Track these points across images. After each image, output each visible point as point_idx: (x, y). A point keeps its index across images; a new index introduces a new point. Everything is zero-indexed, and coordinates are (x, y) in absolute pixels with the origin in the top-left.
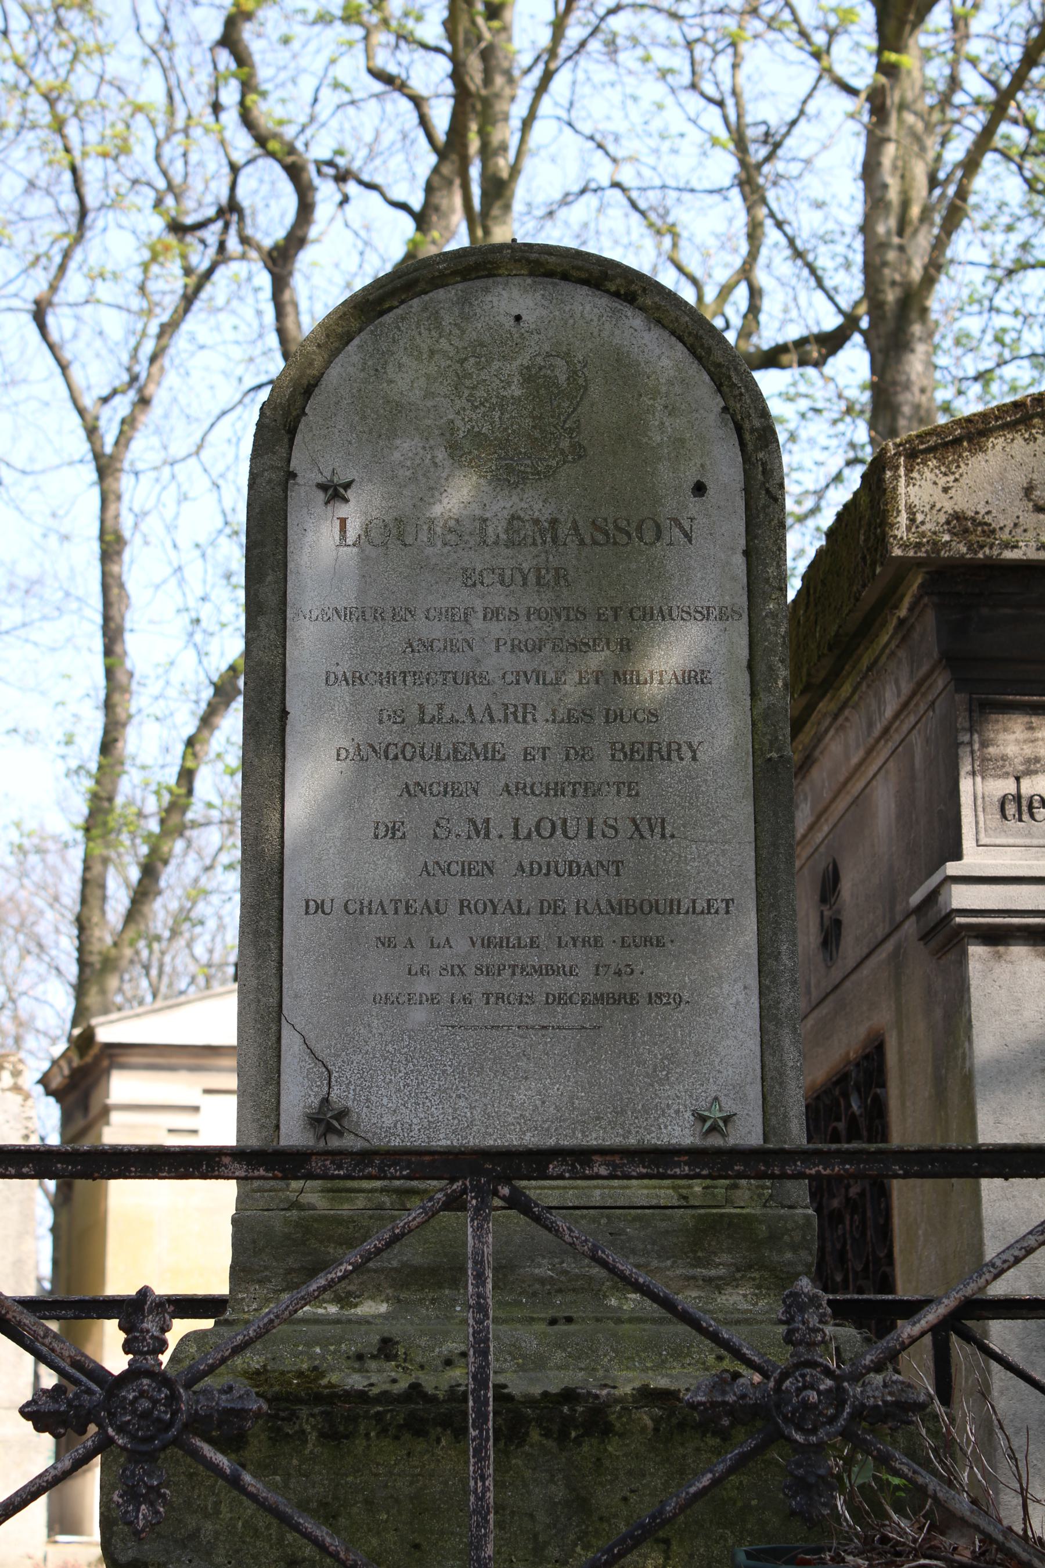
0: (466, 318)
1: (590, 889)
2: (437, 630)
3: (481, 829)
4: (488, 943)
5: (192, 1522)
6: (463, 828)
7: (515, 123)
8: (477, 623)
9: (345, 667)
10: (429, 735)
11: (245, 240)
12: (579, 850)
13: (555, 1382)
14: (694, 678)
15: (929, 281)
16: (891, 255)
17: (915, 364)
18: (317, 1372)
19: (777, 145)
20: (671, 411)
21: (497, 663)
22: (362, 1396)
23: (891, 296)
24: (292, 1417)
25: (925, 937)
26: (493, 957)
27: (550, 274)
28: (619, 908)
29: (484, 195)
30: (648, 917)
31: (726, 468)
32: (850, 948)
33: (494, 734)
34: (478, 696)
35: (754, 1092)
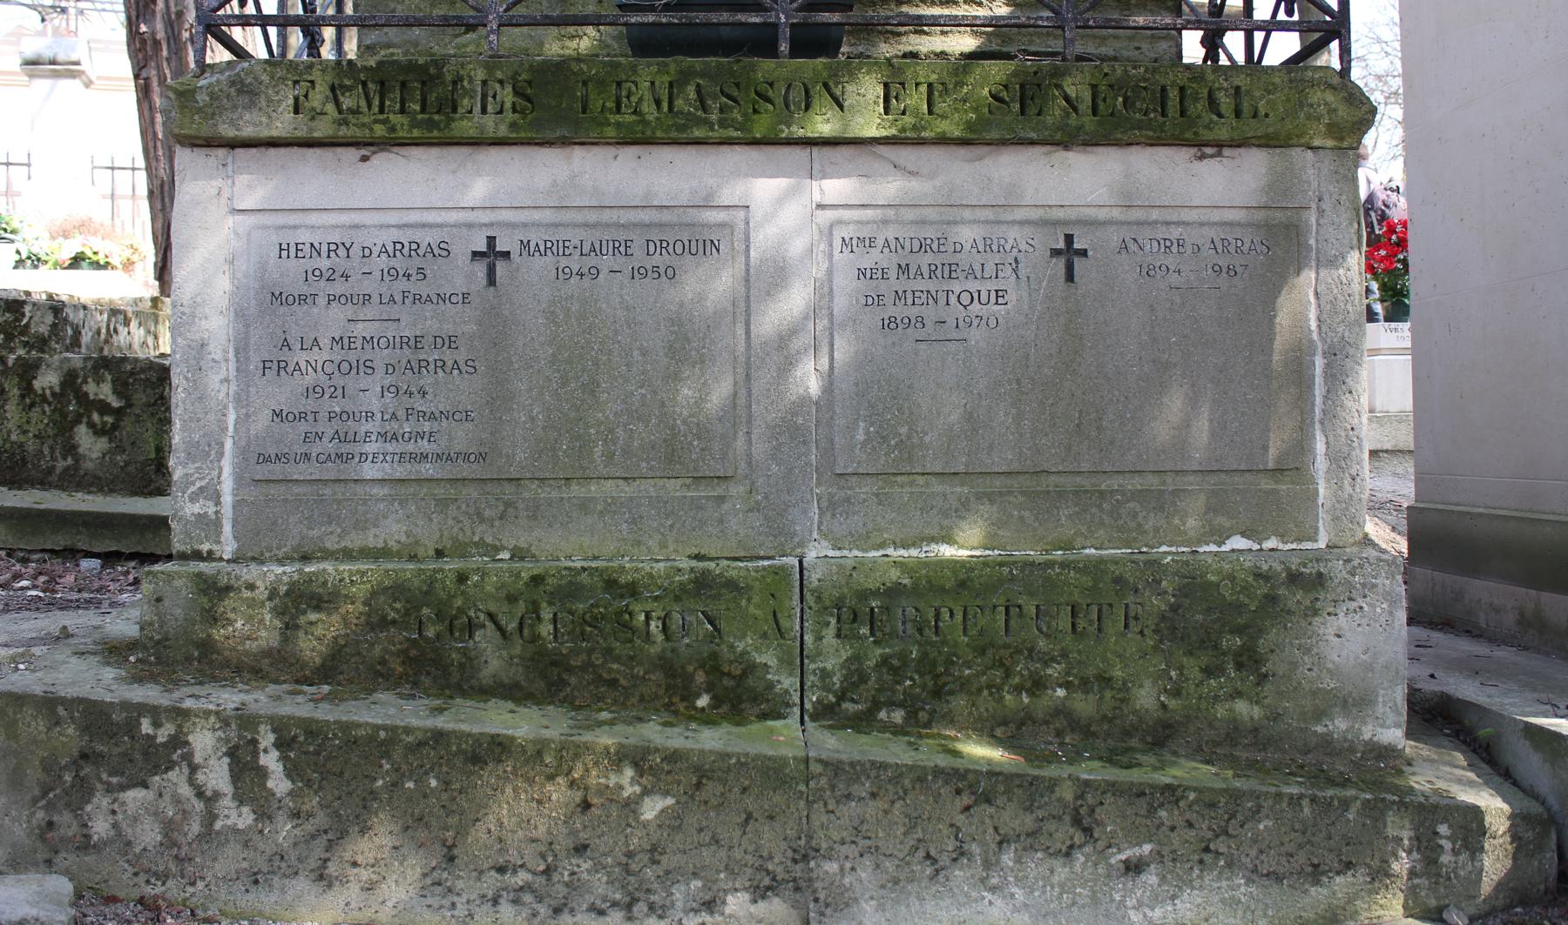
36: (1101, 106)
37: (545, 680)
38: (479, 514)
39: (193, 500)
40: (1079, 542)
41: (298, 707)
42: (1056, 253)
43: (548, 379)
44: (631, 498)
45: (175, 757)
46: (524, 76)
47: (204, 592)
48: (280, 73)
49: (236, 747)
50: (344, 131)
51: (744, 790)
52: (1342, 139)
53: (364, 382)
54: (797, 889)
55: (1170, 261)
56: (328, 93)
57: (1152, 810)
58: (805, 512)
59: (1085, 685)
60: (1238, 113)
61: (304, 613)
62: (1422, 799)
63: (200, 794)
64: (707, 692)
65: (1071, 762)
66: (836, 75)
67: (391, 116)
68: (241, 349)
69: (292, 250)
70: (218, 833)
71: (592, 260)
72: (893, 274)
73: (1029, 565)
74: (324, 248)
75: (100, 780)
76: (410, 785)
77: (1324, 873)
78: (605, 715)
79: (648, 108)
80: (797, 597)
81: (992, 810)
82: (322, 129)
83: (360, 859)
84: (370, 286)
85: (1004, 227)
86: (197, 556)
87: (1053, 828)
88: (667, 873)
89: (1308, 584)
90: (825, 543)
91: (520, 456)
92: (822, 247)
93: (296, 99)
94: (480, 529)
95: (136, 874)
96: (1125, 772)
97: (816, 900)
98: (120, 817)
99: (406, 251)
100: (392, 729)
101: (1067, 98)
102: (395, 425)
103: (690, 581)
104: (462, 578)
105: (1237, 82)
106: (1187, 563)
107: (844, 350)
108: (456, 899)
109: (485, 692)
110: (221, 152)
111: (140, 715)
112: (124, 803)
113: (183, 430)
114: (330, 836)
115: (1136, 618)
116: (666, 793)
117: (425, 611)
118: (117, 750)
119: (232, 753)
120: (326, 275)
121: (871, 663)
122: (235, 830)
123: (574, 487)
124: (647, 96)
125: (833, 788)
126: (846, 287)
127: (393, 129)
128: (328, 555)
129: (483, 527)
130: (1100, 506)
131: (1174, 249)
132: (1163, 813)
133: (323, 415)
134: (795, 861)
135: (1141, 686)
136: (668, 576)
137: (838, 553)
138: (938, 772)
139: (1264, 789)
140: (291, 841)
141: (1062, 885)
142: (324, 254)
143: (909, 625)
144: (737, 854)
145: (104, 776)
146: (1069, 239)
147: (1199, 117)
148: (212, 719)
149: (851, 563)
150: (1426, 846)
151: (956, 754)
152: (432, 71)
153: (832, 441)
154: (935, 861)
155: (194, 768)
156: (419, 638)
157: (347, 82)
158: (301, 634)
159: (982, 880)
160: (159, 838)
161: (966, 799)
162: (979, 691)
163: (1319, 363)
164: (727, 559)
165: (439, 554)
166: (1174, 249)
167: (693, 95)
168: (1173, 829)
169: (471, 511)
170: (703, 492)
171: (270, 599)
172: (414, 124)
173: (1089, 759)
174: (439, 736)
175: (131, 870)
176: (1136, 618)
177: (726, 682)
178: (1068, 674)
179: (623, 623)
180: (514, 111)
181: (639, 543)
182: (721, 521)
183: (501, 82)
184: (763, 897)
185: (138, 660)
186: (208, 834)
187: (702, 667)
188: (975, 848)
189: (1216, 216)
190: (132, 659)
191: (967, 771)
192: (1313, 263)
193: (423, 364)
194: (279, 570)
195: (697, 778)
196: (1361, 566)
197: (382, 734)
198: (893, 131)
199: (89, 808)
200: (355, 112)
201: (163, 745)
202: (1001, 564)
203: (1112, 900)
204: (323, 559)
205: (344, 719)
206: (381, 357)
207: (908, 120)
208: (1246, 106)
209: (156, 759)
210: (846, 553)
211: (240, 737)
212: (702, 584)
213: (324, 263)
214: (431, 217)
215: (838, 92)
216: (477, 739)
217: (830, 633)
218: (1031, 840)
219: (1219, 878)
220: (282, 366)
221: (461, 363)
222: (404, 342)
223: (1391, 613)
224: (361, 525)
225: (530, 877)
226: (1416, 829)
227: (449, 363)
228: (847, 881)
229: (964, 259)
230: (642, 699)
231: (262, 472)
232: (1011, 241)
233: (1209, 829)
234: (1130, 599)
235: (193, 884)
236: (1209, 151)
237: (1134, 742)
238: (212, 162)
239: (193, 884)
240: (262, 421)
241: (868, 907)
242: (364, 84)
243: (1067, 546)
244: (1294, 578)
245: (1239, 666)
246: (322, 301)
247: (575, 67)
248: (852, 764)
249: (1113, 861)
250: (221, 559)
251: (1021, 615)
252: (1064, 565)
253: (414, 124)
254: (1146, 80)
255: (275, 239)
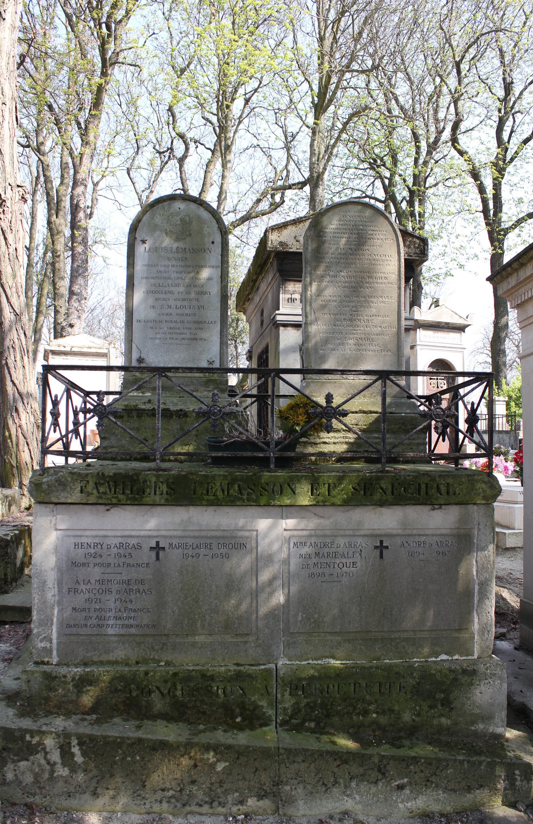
0: (169, 208)
1: (189, 319)
2: (162, 269)
3: (170, 307)
4: (170, 328)
5: (114, 430)
6: (167, 307)
7: (232, 132)
8: (170, 268)
9: (145, 276)
10: (160, 289)
11: (173, 156)
12: (187, 311)
13: (178, 408)
14: (209, 279)
15: (323, 173)
16: (316, 166)
17: (320, 190)
18: (137, 405)
19: (294, 138)
20: (208, 227)
21: (173, 275)
22: (144, 410)
23: (315, 175)
24: (132, 413)
25: (273, 325)
26: (171, 331)
27: (186, 200)
28: (195, 322)
29: (225, 149)
30: (200, 324)
31: (218, 239)
32: (265, 326)
33: (172, 289)
34: (170, 282)
35: (218, 357)
36: (395, 492)
37: (177, 713)
38: (153, 648)
39: (41, 641)
40: (383, 657)
41: (86, 729)
42: (376, 547)
43: (180, 597)
44: (211, 642)
45: (39, 749)
46: (171, 480)
47: (47, 679)
48: (75, 477)
49: (63, 745)
50: (100, 501)
51: (255, 760)
52: (488, 501)
53: (108, 597)
54: (274, 796)
55: (420, 550)
56: (94, 485)
57: (408, 766)
58: (278, 647)
59: (384, 712)
60: (448, 493)
61: (85, 686)
62: (509, 761)
63: (48, 763)
64: (240, 716)
65: (378, 746)
66: (292, 480)
67: (119, 496)
68: (60, 583)
69: (80, 545)
70: (55, 778)
71: (197, 551)
72: (313, 556)
73: (363, 668)
74: (92, 545)
75: (10, 758)
76: (129, 759)
77: (472, 789)
78: (202, 727)
79: (219, 494)
80: (275, 680)
81: (348, 766)
82: (92, 500)
83: (109, 787)
84: (110, 560)
85: (356, 538)
86: (43, 663)
87: (370, 773)
88: (226, 790)
89: (469, 675)
90: (286, 659)
91: (169, 626)
92: (286, 545)
93: (81, 487)
94: (153, 653)
95: (23, 794)
96: (398, 750)
97: (282, 800)
98: (18, 772)
99: (124, 546)
100: (122, 738)
101: (382, 489)
102: (120, 614)
103: (234, 674)
104: (146, 673)
105: (448, 481)
106: (423, 666)
107: (294, 589)
108: (146, 801)
109: (154, 717)
110: (51, 506)
111: (26, 733)
112: (19, 767)
113: (37, 614)
114: (98, 778)
115: (404, 687)
116: (226, 761)
117: (132, 686)
118: (17, 747)
119: (61, 747)
120: (93, 555)
121: (303, 705)
122: (62, 776)
123: (190, 637)
124: (219, 489)
125: (288, 758)
126: (294, 563)
127: (119, 500)
128: (94, 663)
129: (154, 653)
130: (391, 644)
131: (422, 545)
132: (412, 767)
133: (92, 610)
134: (274, 786)
135: (405, 713)
136: (225, 673)
137: (290, 663)
138: (328, 752)
139: (450, 757)
140: (83, 780)
141: (374, 794)
142: (92, 547)
143: (317, 691)
144: (252, 783)
145: (12, 757)
146: (381, 542)
147: (433, 495)
148: (54, 735)
149: (295, 667)
150: (510, 778)
151: (334, 743)
152: (135, 478)
153: (289, 620)
154: (326, 785)
155: (46, 753)
156: (129, 697)
157: (102, 482)
158: (84, 695)
159: (344, 792)
160: (32, 780)
161: (338, 763)
162: (344, 715)
163: (477, 587)
164: (249, 665)
165: (137, 663)
166: (422, 545)
167: (236, 488)
168: (415, 773)
169: (150, 646)
170: (240, 639)
171: (72, 681)
172: (128, 499)
173: (385, 743)
174: (140, 740)
175: (21, 792)
176: (404, 687)
177: (248, 712)
178: (377, 708)
179: (208, 691)
180: (167, 494)
181: (214, 659)
182: (246, 651)
183: (162, 482)
184: (262, 799)
185: (20, 705)
186: (52, 778)
187: (238, 707)
188: (341, 781)
189: (438, 532)
190: (18, 704)
191: (339, 752)
192: (475, 549)
193: (131, 590)
194: (76, 670)
195: (236, 754)
196: (490, 666)
197: (119, 740)
198: (314, 503)
199: (5, 769)
200: (105, 493)
201: (35, 744)
202: (353, 668)
203: (392, 800)
204: (92, 664)
205: (104, 734)
206: (115, 587)
207: (320, 498)
208: (451, 490)
209: (31, 750)
210: (293, 662)
211: (64, 741)
212: (239, 676)
213: (92, 551)
214: (134, 533)
215: (293, 487)
216: (155, 742)
217: (287, 694)
218: (362, 778)
219: (433, 791)
220: (76, 591)
221: (146, 590)
222: (124, 582)
223: (501, 684)
224: (107, 652)
225: (174, 793)
226: (507, 772)
227: (141, 590)
228: (293, 793)
229: (340, 550)
230: (215, 719)
231: (68, 631)
232: (359, 543)
233: (429, 773)
234: (402, 680)
235: (45, 797)
236: (436, 507)
237: (402, 734)
238: (48, 509)
239: (45, 797)
240: (68, 613)
241: (301, 803)
242: (108, 482)
243: (378, 659)
244: (464, 672)
245: (443, 705)
246: (91, 565)
247: (191, 477)
248: (296, 750)
249: (393, 785)
250: (52, 664)
251: (360, 687)
252: (377, 668)
253: (128, 499)
254: (413, 481)
255: (73, 540)
